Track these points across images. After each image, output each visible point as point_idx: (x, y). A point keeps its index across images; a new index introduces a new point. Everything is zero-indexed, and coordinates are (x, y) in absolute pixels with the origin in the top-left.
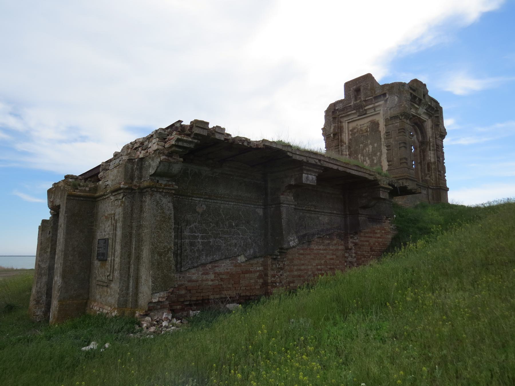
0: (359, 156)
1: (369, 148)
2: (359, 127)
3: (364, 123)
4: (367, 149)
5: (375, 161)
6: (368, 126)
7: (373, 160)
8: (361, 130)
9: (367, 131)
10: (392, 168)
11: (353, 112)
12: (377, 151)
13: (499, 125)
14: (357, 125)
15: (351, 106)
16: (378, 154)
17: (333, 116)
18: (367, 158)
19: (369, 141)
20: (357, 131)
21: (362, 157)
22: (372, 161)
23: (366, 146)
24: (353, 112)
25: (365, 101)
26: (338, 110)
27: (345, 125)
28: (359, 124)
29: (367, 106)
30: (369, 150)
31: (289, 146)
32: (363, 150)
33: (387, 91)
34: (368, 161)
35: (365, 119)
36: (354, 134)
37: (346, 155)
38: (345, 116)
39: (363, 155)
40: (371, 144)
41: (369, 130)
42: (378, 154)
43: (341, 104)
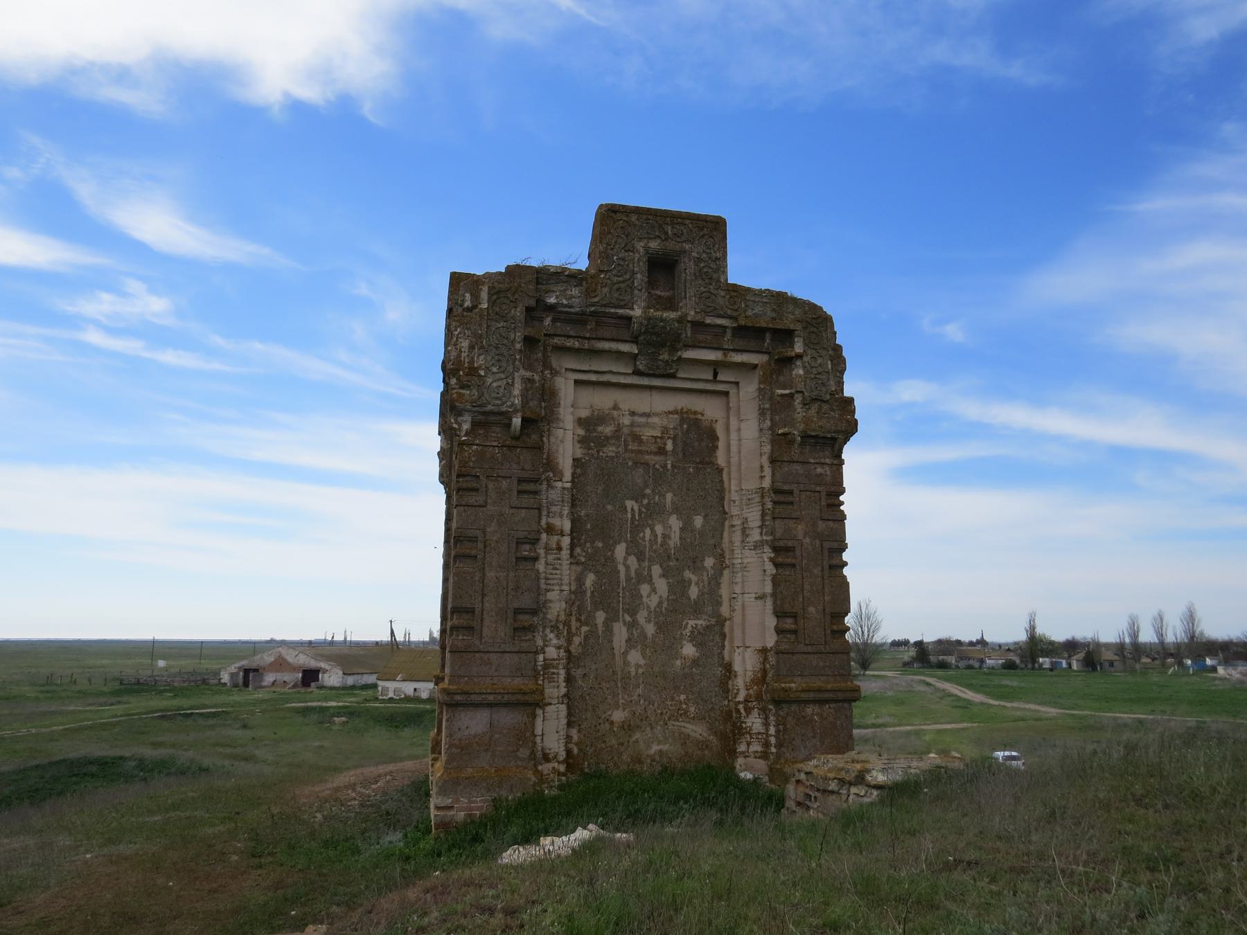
0: (620, 550)
1: (667, 527)
2: (626, 421)
3: (651, 409)
4: (659, 529)
5: (694, 592)
6: (665, 430)
7: (685, 584)
8: (637, 438)
9: (661, 451)
10: (801, 648)
11: (625, 348)
12: (704, 549)
13: (258, 346)
14: (616, 407)
15: (629, 318)
16: (709, 562)
17: (530, 331)
18: (656, 570)
19: (669, 496)
20: (617, 435)
21: (632, 561)
22: (679, 587)
23: (654, 512)
24: (625, 348)
25: (697, 325)
26: (552, 308)
27: (565, 387)
28: (625, 406)
29: (694, 346)
30: (666, 537)
31: (75, 71)
32: (637, 528)
33: (799, 327)
34: (662, 586)
35: (646, 395)
36: (602, 442)
37: (562, 534)
38: (578, 351)
39: (636, 549)
40: (676, 510)
41: (669, 446)
42: (709, 562)
43: (575, 291)
